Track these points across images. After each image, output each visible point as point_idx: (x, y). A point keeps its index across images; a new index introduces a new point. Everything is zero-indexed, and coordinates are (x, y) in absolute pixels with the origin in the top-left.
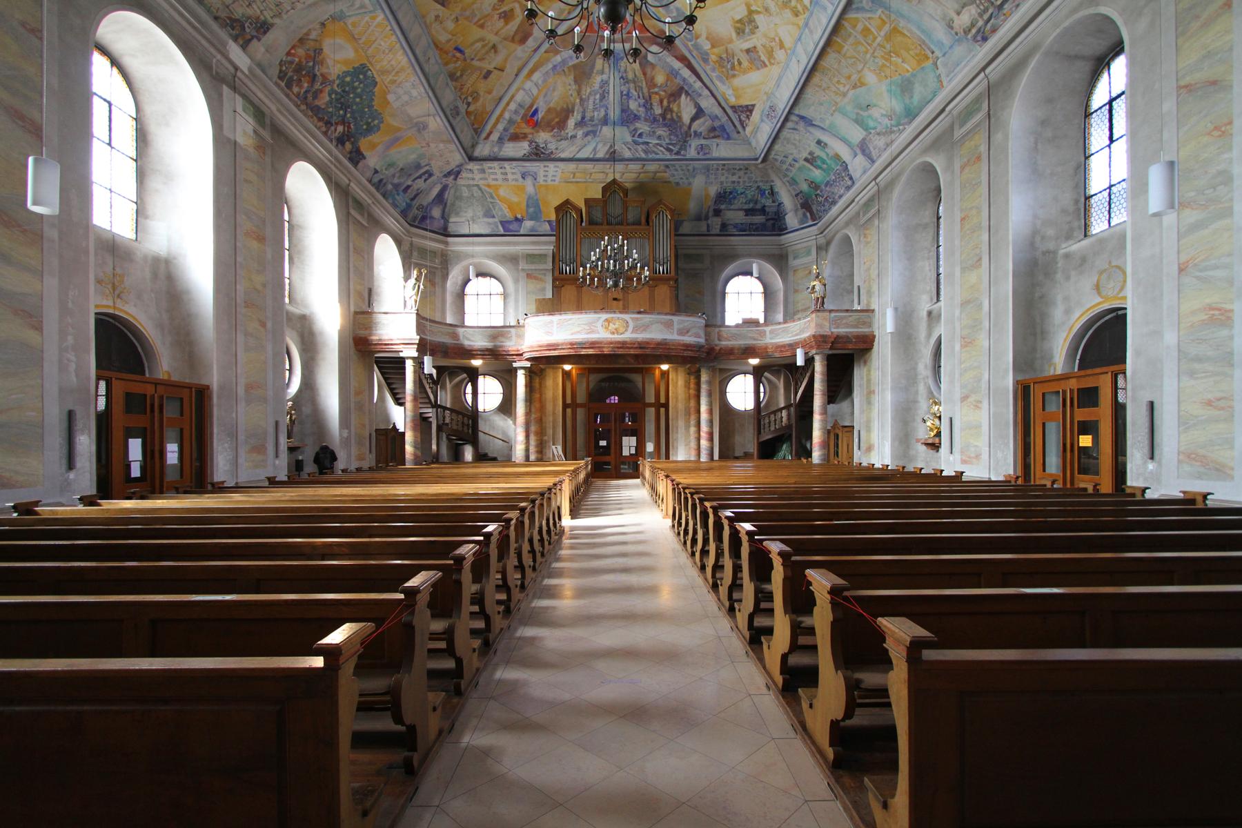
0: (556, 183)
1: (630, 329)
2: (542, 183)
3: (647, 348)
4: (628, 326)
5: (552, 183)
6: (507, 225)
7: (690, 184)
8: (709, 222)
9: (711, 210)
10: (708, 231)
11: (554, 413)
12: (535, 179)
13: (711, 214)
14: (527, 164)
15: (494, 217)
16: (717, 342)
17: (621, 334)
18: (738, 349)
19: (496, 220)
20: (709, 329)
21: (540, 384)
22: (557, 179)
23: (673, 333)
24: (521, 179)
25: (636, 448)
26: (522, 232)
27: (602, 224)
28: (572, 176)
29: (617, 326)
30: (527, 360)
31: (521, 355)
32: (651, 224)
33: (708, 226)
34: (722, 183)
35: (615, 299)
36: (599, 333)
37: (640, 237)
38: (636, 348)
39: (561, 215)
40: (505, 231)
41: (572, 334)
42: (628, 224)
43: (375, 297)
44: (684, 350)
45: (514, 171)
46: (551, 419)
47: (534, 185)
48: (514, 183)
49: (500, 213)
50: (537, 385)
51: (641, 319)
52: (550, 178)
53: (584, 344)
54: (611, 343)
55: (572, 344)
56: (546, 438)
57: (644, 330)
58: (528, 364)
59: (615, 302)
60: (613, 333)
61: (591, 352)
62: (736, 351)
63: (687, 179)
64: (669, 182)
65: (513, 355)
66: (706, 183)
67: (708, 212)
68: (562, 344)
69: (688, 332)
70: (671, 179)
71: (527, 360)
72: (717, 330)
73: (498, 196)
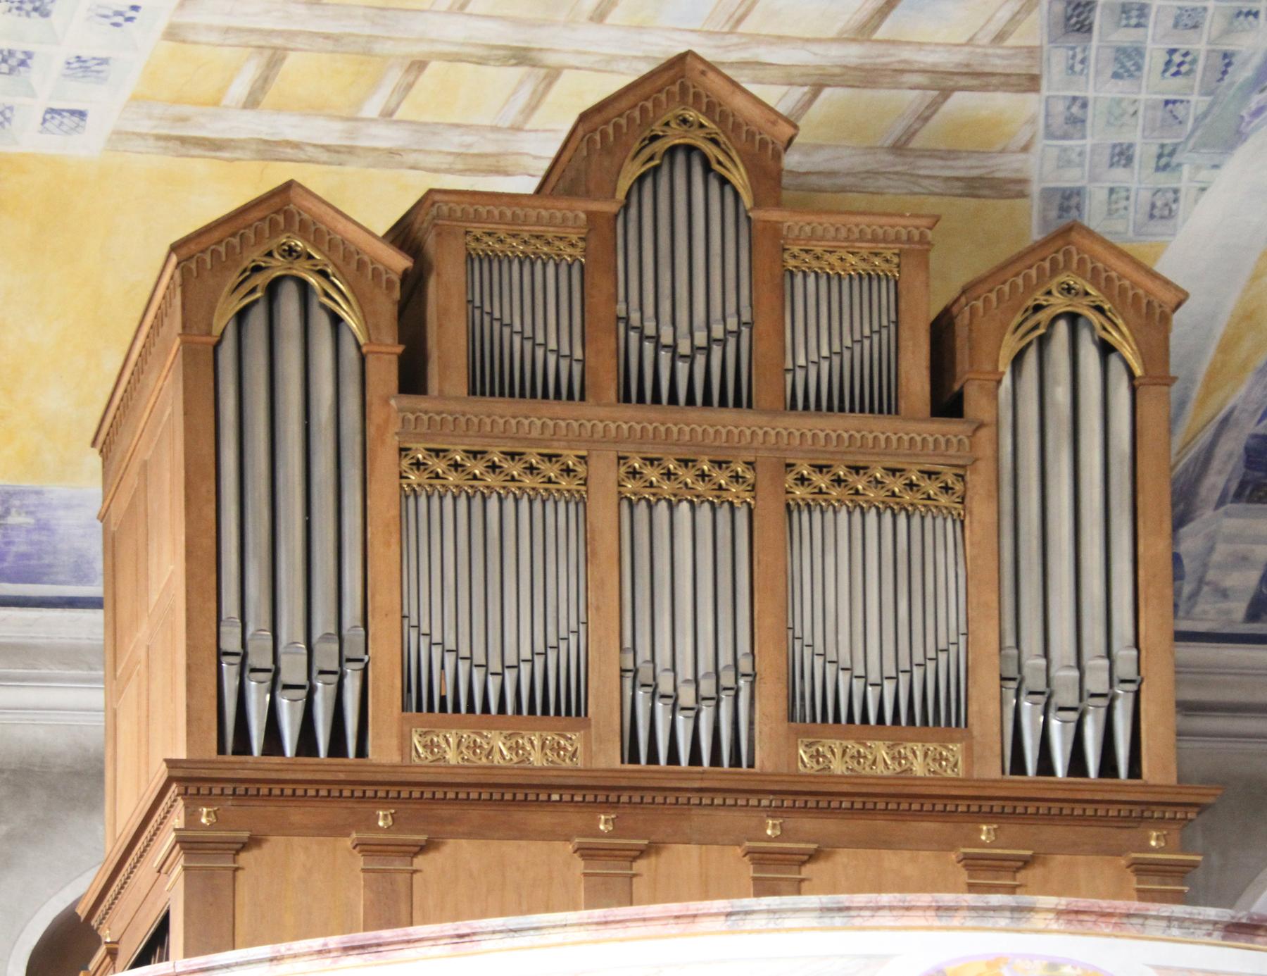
27: (576, 393)
28: (240, 89)
37: (892, 504)
39: (223, 318)
43: (838, 920)
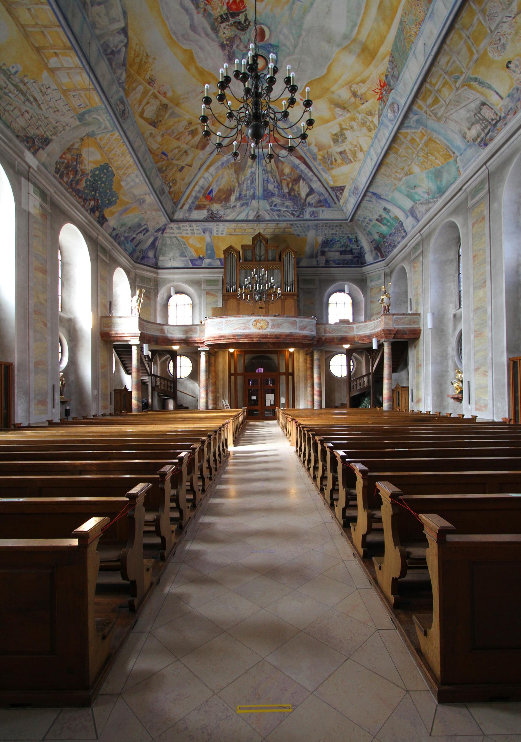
0: (224, 235)
1: (270, 326)
2: (215, 235)
3: (280, 338)
4: (268, 325)
5: (222, 235)
6: (194, 262)
7: (306, 235)
8: (318, 259)
9: (319, 251)
10: (318, 264)
11: (223, 379)
12: (211, 233)
13: (319, 254)
14: (206, 224)
15: (186, 256)
16: (323, 334)
17: (264, 329)
18: (337, 338)
19: (188, 258)
20: (319, 326)
21: (215, 361)
22: (225, 233)
23: (296, 329)
24: (202, 233)
25: (274, 401)
26: (203, 266)
27: (252, 261)
28: (233, 231)
29: (262, 325)
30: (207, 346)
31: (203, 343)
32: (282, 260)
33: (317, 261)
34: (325, 234)
35: (260, 308)
36: (250, 329)
38: (273, 338)
40: (193, 265)
41: (234, 330)
42: (268, 261)
44: (304, 339)
45: (198, 228)
46: (222, 382)
47: (210, 237)
48: (198, 235)
49: (190, 254)
50: (213, 362)
51: (277, 320)
52: (220, 232)
53: (242, 336)
54: (258, 335)
55: (234, 336)
56: (218, 395)
57: (279, 327)
58: (207, 349)
59: (260, 309)
60: (259, 329)
61: (246, 341)
62: (335, 340)
63: (304, 232)
64: (294, 234)
65: (198, 343)
66: (316, 235)
67: (317, 252)
68: (228, 336)
69: (305, 328)
70: (295, 233)
71: (207, 346)
72: (323, 326)
73: (188, 244)
